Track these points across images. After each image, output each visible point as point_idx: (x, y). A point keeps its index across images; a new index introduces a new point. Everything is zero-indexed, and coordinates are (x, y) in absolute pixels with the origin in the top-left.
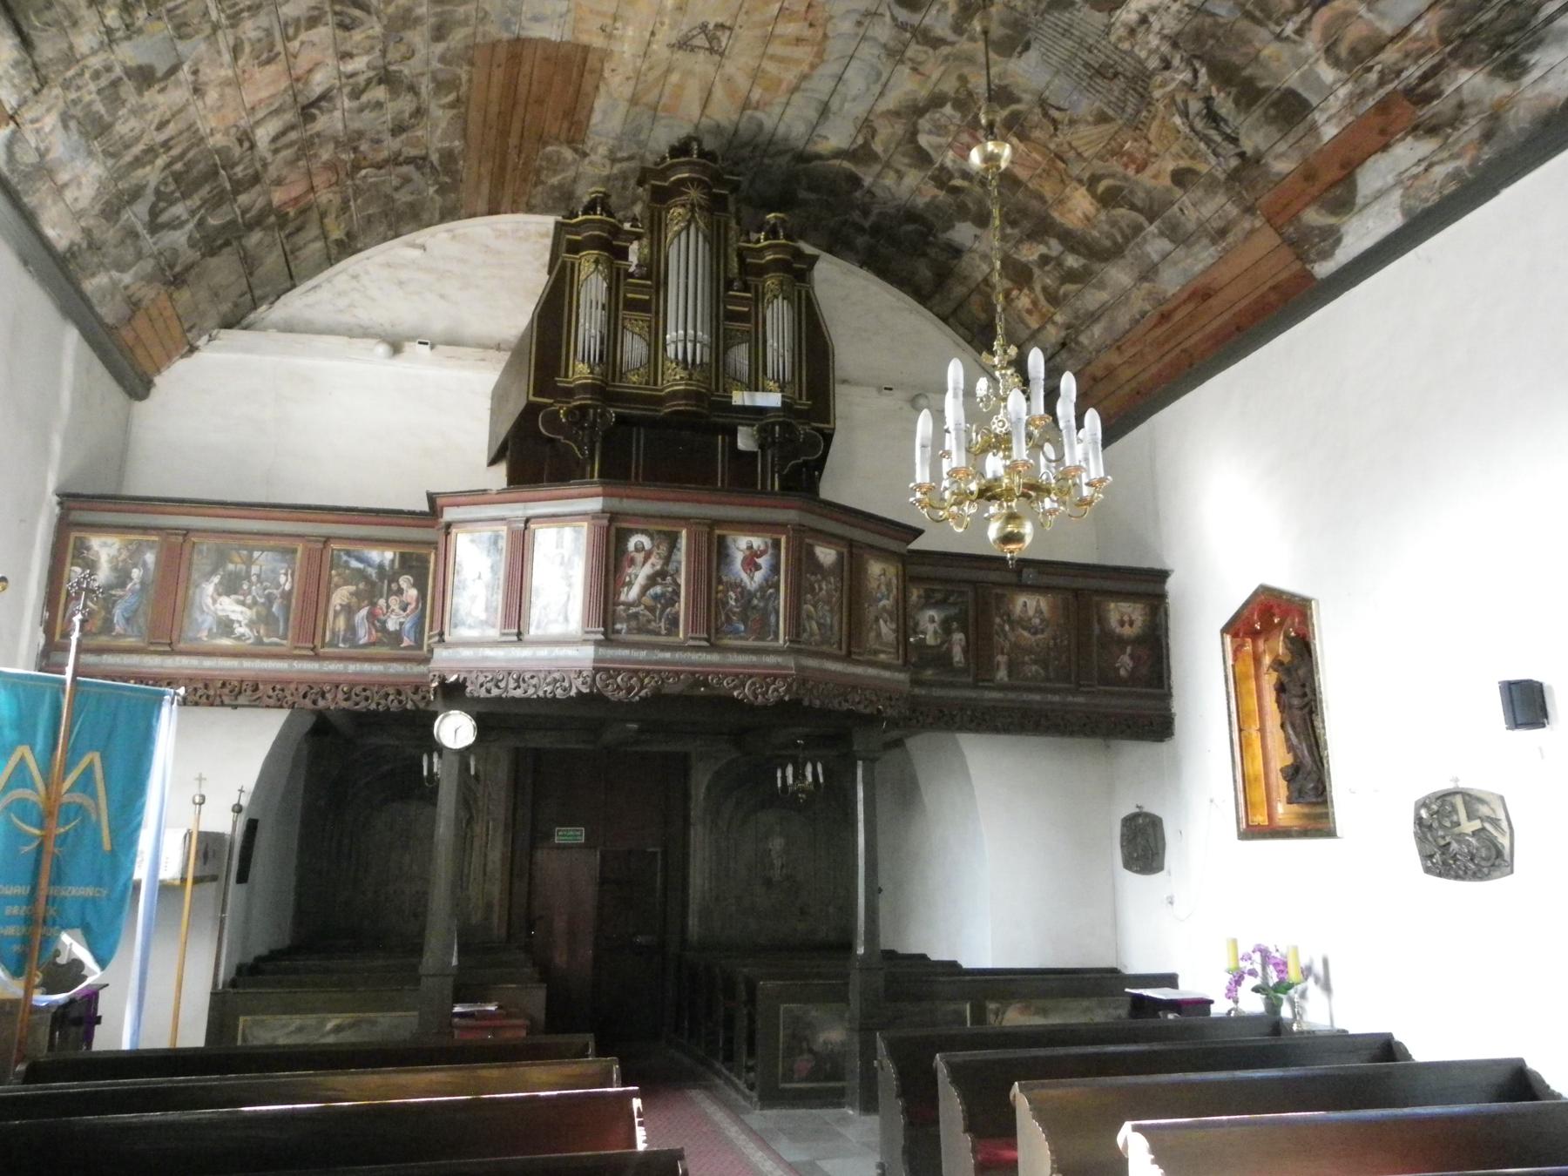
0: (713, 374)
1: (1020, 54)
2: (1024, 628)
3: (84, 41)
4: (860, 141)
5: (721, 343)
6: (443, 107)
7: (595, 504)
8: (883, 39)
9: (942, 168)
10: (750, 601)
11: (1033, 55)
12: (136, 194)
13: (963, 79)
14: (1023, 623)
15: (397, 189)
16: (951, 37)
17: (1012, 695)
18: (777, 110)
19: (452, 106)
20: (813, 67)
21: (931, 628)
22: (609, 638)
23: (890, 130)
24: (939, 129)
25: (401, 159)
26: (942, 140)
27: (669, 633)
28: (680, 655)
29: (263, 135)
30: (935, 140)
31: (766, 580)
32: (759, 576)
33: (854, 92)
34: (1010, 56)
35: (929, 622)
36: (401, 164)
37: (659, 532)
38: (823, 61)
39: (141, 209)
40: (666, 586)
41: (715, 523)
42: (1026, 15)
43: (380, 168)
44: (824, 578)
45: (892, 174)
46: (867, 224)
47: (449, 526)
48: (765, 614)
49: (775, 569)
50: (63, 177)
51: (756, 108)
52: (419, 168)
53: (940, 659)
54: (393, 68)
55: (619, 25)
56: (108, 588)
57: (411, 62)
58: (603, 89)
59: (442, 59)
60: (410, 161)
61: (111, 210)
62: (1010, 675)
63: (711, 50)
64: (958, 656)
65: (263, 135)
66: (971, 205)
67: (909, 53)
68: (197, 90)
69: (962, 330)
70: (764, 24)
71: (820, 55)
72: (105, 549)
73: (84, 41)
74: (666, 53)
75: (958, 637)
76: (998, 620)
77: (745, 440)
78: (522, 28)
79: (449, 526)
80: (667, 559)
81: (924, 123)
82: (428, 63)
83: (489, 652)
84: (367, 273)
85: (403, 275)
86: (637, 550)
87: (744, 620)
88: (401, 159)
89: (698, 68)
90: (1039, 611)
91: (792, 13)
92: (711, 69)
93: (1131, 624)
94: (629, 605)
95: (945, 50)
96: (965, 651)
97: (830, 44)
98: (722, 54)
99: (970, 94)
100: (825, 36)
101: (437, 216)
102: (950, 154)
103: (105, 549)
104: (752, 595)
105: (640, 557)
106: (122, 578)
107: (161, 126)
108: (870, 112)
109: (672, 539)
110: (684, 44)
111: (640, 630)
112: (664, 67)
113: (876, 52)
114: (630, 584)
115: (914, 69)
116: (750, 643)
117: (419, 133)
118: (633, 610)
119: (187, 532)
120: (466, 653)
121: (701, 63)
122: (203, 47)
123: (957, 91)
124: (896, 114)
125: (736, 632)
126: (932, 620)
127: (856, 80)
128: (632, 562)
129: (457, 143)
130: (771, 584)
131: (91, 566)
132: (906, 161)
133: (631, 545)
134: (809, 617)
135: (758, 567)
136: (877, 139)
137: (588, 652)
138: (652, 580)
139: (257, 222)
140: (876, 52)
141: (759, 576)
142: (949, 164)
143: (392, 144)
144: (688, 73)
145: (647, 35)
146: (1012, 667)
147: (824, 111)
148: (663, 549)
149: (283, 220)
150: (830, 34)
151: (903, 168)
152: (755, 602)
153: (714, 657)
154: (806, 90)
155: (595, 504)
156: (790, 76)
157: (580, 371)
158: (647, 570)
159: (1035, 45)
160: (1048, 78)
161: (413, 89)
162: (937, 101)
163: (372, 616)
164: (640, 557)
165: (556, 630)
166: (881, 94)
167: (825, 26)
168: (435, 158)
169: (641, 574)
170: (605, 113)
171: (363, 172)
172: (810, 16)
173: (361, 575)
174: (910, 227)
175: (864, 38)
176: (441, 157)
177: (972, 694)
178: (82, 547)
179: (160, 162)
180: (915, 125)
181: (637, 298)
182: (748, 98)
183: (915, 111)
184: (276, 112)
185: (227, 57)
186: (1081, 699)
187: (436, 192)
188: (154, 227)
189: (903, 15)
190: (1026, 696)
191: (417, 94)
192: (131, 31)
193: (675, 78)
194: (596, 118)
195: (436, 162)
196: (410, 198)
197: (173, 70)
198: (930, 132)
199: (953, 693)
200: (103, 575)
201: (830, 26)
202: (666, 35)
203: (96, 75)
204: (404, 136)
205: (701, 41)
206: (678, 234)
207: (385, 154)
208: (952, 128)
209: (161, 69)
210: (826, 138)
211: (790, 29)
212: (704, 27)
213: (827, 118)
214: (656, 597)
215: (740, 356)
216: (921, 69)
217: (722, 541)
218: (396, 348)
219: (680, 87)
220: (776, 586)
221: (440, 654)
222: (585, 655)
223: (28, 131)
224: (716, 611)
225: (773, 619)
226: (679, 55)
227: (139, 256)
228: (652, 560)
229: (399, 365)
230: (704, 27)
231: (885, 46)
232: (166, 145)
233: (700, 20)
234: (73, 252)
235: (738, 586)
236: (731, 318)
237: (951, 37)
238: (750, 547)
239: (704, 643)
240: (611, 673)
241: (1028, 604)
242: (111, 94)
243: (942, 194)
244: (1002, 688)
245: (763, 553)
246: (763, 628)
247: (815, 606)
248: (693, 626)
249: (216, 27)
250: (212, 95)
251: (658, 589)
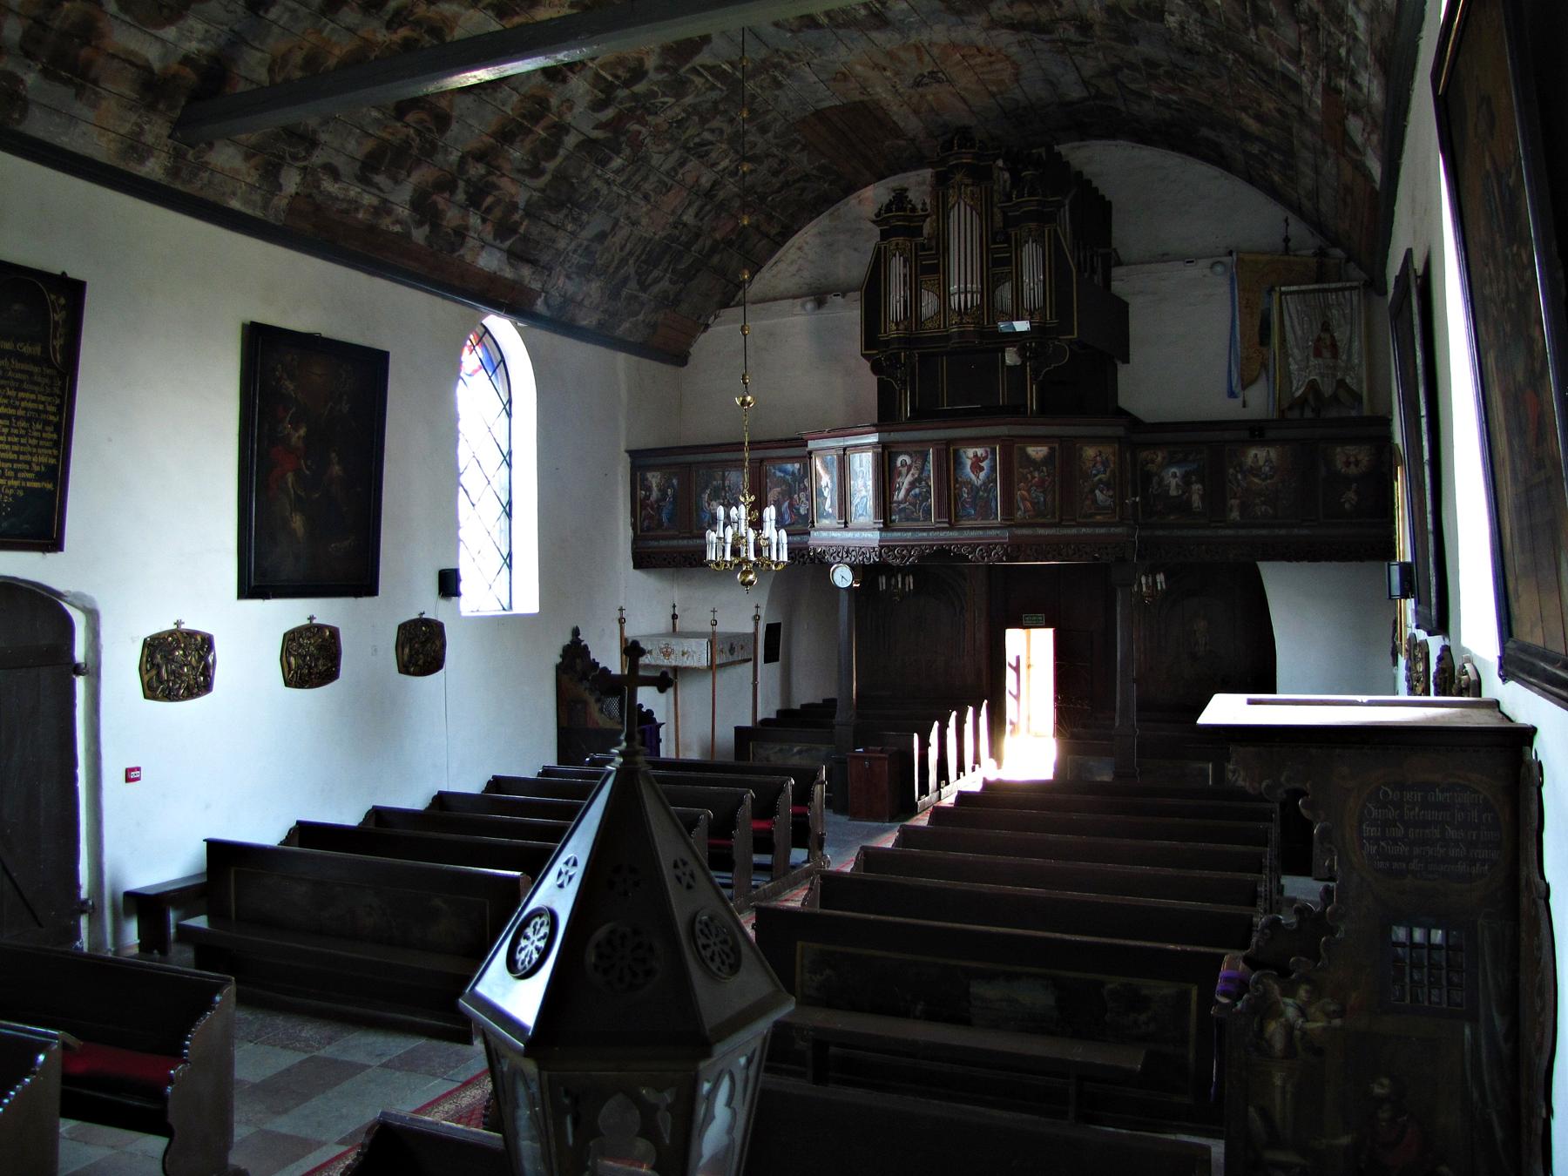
0: (989, 309)
2: (1256, 476)
3: (562, 244)
5: (990, 284)
7: (874, 438)
12: (626, 280)
14: (1255, 471)
17: (1242, 532)
19: (802, 150)
21: (1173, 482)
22: (887, 526)
28: (929, 533)
29: (688, 218)
32: (982, 475)
35: (1172, 478)
39: (633, 285)
41: (949, 442)
47: (810, 453)
48: (987, 502)
49: (993, 469)
50: (579, 298)
53: (1181, 506)
56: (658, 501)
61: (615, 295)
62: (1242, 516)
64: (1196, 501)
65: (688, 218)
68: (634, 223)
72: (654, 479)
73: (562, 244)
75: (1196, 487)
76: (1231, 471)
77: (1011, 357)
79: (810, 453)
80: (922, 470)
83: (834, 534)
87: (974, 506)
90: (1268, 460)
93: (1357, 463)
94: (899, 503)
96: (1202, 498)
103: (654, 479)
104: (978, 489)
105: (904, 470)
106: (663, 491)
107: (622, 249)
109: (924, 457)
116: (979, 523)
119: (689, 465)
120: (824, 534)
122: (626, 208)
126: (1174, 475)
128: (900, 474)
130: (991, 479)
131: (649, 489)
135: (982, 469)
137: (877, 535)
138: (912, 485)
139: (714, 250)
141: (982, 475)
143: (776, 182)
146: (1244, 508)
148: (919, 463)
149: (730, 243)
153: (954, 534)
155: (874, 438)
157: (892, 332)
158: (909, 478)
163: (791, 506)
164: (904, 470)
165: (862, 520)
169: (906, 481)
173: (784, 481)
177: (1208, 533)
178: (644, 479)
179: (631, 262)
181: (929, 267)
184: (690, 205)
185: (642, 203)
186: (1305, 532)
188: (644, 287)
190: (1255, 532)
192: (582, 227)
197: (616, 223)
199: (1192, 533)
200: (655, 494)
203: (575, 251)
209: (607, 228)
214: (916, 496)
215: (1005, 293)
217: (956, 452)
218: (820, 303)
221: (814, 534)
222: (873, 538)
223: (554, 292)
224: (951, 501)
227: (642, 304)
229: (825, 312)
232: (631, 254)
234: (600, 324)
235: (970, 482)
236: (998, 264)
240: (891, 548)
241: (1258, 455)
242: (588, 252)
244: (1235, 525)
246: (986, 512)
247: (1029, 491)
248: (939, 515)
249: (628, 197)
250: (644, 221)
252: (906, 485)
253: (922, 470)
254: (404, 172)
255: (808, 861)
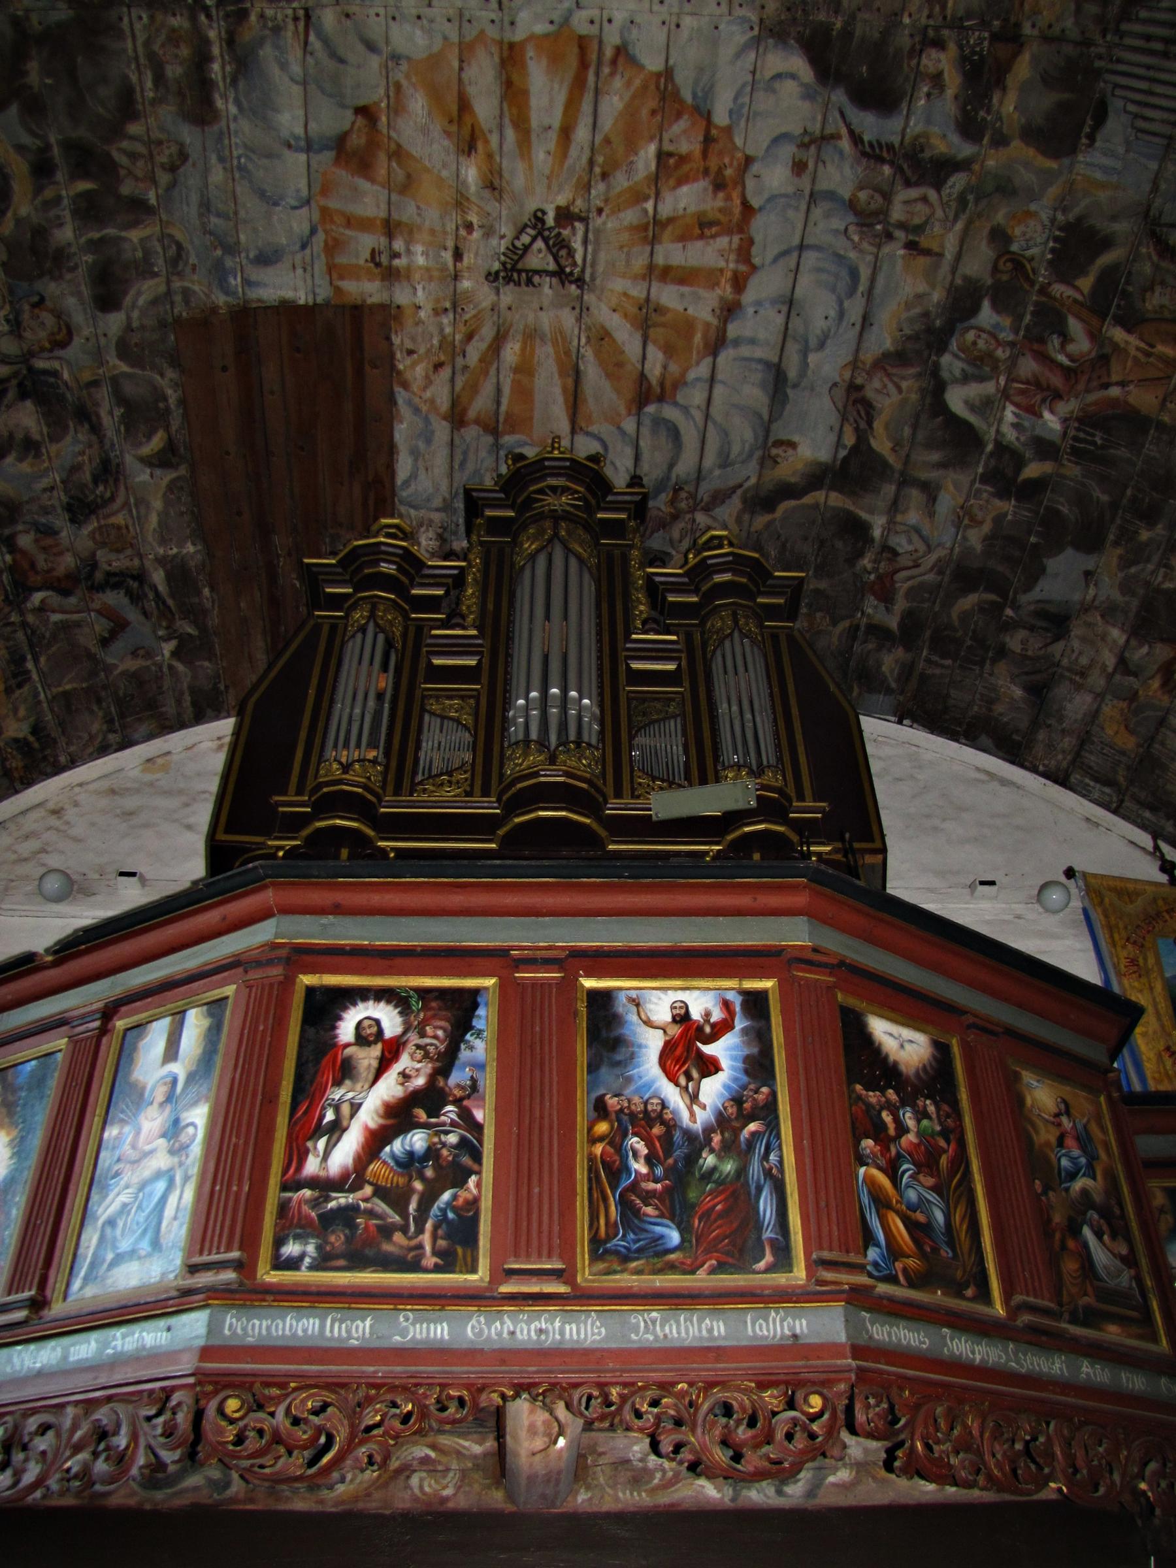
1: (1092, 138)
4: (850, 440)
6: (147, 461)
8: (846, 193)
9: (1002, 448)
10: (692, 1158)
11: (1116, 127)
13: (999, 237)
15: (105, 642)
16: (967, 150)
18: (697, 397)
20: (739, 283)
23: (895, 397)
24: (980, 365)
25: (99, 576)
26: (989, 388)
27: (447, 1262)
30: (974, 390)
31: (737, 1100)
32: (713, 1089)
33: (819, 324)
34: (1073, 151)
36: (101, 588)
37: (424, 993)
38: (754, 268)
40: (439, 1130)
42: (1087, 43)
43: (66, 593)
44: (907, 1100)
45: (915, 494)
46: (893, 623)
48: (739, 1194)
49: (758, 1066)
51: (661, 399)
52: (135, 598)
54: (40, 364)
55: (398, 245)
57: (69, 353)
58: (401, 395)
59: (124, 349)
60: (115, 580)
63: (560, 275)
66: (1065, 510)
67: (897, 213)
69: (1097, 789)
70: (638, 197)
71: (744, 253)
74: (485, 296)
78: (247, 282)
81: (951, 364)
82: (98, 356)
84: (76, 804)
85: (130, 803)
86: (361, 1039)
87: (676, 1206)
88: (99, 576)
89: (545, 320)
91: (683, 159)
92: (568, 318)
94: (325, 1186)
95: (958, 182)
97: (759, 227)
98: (580, 282)
99: (1018, 264)
100: (748, 210)
101: (189, 711)
102: (1009, 414)
104: (696, 1143)
105: (367, 1058)
108: (855, 364)
109: (460, 1009)
110: (512, 271)
111: (357, 1261)
112: (487, 332)
113: (837, 224)
114: (337, 1129)
115: (911, 246)
117: (120, 519)
118: (340, 1200)
121: (545, 310)
123: (995, 269)
124: (897, 358)
125: (655, 1249)
127: (820, 308)
129: (190, 548)
132: (935, 457)
133: (346, 1030)
134: (881, 1202)
135: (710, 1067)
136: (877, 425)
138: (399, 1116)
140: (837, 224)
141: (713, 1089)
142: (1010, 435)
144: (531, 336)
145: (448, 256)
147: (778, 382)
148: (437, 1034)
150: (755, 202)
151: (933, 475)
152: (709, 1160)
154: (737, 342)
156: (702, 307)
158: (388, 1088)
159: (1116, 104)
160: (1154, 166)
161: (85, 416)
162: (963, 303)
166: (866, 321)
167: (740, 181)
168: (158, 577)
170: (415, 453)
171: (38, 597)
172: (713, 164)
174: (969, 601)
175: (813, 197)
176: (169, 577)
180: (935, 371)
182: (642, 376)
183: (929, 339)
187: (175, 654)
189: (869, 124)
191: (96, 429)
193: (511, 352)
194: (404, 467)
195: (162, 588)
196: (131, 665)
198: (966, 379)
201: (750, 184)
202: (484, 252)
204: (93, 525)
205: (539, 258)
206: (533, 557)
207: (68, 562)
208: (1000, 353)
210: (792, 445)
211: (687, 198)
212: (538, 218)
213: (785, 399)
214: (410, 1162)
216: (924, 242)
219: (525, 369)
220: (768, 1112)
225: (766, 1206)
226: (508, 295)
228: (405, 1062)
230: (538, 218)
231: (851, 205)
233: (532, 205)
235: (652, 1120)
237: (967, 150)
238: (682, 1017)
239: (562, 1289)
243: (1008, 507)
245: (720, 1030)
247: (892, 1172)
251: (418, 1140)
252: (368, 1116)
253: (446, 1061)
254: (672, 182)
255: (1164, 1465)
